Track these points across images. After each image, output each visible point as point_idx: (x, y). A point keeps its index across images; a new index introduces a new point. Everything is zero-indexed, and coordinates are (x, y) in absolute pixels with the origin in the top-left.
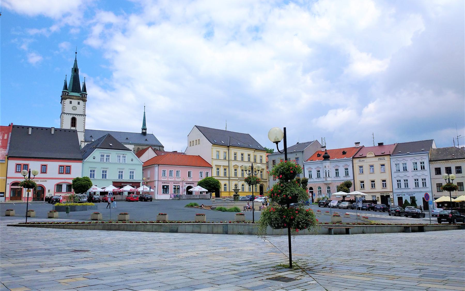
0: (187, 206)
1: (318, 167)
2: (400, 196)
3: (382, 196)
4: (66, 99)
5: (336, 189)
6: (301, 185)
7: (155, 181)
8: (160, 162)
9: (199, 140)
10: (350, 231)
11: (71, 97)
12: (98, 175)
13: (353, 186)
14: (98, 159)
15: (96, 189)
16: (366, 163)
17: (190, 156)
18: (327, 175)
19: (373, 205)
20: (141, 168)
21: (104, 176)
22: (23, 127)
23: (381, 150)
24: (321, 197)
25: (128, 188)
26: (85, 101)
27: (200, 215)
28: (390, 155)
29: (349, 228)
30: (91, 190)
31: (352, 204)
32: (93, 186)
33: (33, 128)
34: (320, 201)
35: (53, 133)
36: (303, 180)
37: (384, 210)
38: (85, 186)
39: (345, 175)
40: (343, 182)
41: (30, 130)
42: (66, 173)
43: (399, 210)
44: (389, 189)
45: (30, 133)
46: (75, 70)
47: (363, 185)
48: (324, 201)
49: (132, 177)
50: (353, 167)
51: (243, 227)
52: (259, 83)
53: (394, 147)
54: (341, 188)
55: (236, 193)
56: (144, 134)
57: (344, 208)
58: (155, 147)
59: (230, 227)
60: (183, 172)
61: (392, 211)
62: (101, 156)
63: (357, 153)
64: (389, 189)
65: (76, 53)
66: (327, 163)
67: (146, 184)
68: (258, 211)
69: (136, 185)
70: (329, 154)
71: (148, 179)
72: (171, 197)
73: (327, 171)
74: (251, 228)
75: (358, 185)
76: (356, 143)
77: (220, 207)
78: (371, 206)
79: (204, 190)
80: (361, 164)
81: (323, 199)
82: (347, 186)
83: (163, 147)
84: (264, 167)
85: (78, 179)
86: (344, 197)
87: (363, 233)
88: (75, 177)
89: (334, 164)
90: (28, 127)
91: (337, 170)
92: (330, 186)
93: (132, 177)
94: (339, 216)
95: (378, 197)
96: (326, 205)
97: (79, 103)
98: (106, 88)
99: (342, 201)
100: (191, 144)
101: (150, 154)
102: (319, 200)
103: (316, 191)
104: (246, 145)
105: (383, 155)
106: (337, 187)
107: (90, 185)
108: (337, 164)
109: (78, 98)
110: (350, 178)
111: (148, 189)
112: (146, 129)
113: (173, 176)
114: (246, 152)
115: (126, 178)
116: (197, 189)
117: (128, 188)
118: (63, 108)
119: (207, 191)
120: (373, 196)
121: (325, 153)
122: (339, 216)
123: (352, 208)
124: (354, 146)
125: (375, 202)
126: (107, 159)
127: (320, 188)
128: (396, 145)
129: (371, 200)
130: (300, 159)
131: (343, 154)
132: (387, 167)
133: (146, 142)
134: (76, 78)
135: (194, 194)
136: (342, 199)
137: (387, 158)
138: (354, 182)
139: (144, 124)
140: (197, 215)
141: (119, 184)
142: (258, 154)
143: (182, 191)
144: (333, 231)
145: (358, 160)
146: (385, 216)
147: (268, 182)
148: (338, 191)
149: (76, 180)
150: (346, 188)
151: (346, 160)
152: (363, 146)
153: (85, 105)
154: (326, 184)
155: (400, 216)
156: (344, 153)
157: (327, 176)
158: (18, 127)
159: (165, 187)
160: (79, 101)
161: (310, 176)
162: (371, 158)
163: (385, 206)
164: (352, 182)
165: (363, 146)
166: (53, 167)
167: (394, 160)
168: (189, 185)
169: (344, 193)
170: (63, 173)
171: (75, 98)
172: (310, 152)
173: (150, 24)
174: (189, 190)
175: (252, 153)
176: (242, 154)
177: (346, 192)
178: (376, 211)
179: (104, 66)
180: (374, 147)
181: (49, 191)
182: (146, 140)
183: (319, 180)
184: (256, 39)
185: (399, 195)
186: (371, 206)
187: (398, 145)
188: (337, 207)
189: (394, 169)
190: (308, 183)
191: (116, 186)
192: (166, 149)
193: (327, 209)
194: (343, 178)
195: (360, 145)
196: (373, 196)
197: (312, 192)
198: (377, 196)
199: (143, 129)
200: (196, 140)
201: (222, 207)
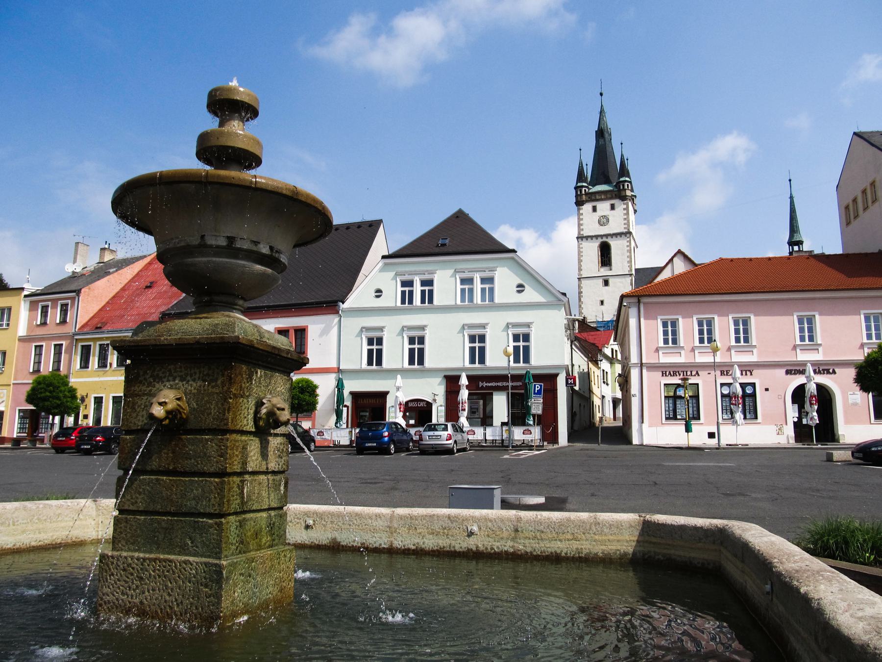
21: (417, 356)
46: (602, 134)
93: (522, 353)
112: (799, 243)
113: (682, 341)
139: (794, 228)
160: (613, 202)
164: (600, 240)
199: (791, 243)
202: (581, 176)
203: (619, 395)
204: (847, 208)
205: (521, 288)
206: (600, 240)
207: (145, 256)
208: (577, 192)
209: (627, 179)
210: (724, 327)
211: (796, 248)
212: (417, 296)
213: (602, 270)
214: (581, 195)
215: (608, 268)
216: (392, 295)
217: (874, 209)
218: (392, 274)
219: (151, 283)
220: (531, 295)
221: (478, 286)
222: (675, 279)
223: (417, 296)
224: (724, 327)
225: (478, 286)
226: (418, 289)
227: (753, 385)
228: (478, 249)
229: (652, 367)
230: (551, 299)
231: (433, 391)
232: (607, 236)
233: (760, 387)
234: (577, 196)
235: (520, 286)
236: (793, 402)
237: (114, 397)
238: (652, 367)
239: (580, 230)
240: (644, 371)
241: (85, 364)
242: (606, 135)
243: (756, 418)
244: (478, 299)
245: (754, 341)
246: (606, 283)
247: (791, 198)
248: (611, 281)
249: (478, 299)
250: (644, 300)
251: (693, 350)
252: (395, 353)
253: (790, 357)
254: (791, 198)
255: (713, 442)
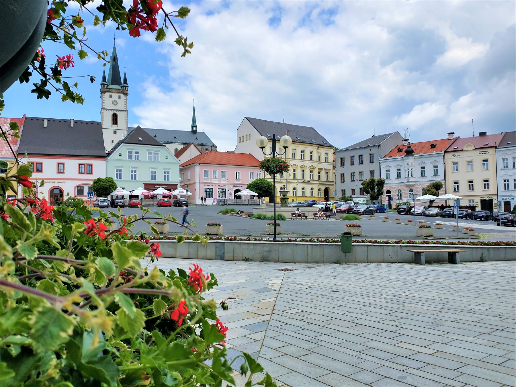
0: (221, 212)
1: (398, 165)
2: (508, 200)
3: (482, 201)
4: (105, 92)
5: (421, 192)
6: (376, 187)
7: (196, 183)
8: (202, 161)
9: (250, 135)
10: (458, 257)
11: (110, 90)
12: (126, 175)
13: (443, 188)
14: (125, 156)
15: (121, 191)
16: (462, 159)
17: (238, 154)
18: (410, 174)
19: (470, 211)
20: (178, 168)
21: (133, 177)
22: (38, 119)
23: (483, 143)
24: (401, 202)
25: (160, 191)
26: (126, 94)
27: (213, 225)
28: (496, 147)
29: (455, 252)
30: (115, 193)
31: (445, 211)
32: (119, 189)
33: (49, 120)
34: (400, 207)
35: (72, 125)
36: (378, 182)
37: (487, 218)
38: (107, 188)
39: (433, 174)
40: (431, 182)
41: (45, 122)
42: (87, 173)
43: (513, 218)
44: (492, 190)
45: (45, 126)
47: (458, 186)
48: (405, 207)
49: (167, 178)
50: (444, 164)
51: (252, 247)
52: (331, 75)
53: (502, 136)
54: (429, 190)
55: (284, 196)
56: (194, 132)
57: (432, 216)
58: (207, 147)
59: (229, 247)
60: (230, 172)
61: (502, 219)
62: (129, 152)
63: (450, 146)
64: (492, 190)
65: (114, 39)
66: (410, 160)
67: (186, 187)
68: (312, 220)
69: (171, 187)
70: (413, 148)
71: (189, 180)
72: (213, 202)
73: (410, 169)
74: (266, 249)
75: (450, 186)
76: (449, 134)
77: (259, 213)
78: (469, 213)
79: (254, 193)
80: (455, 160)
81: (404, 204)
82: (436, 188)
83: (216, 147)
84: (331, 167)
85: (99, 180)
86: (431, 202)
87: (482, 260)
88: (96, 178)
89: (419, 161)
90: (43, 119)
91: (423, 168)
92: (414, 188)
93: (167, 178)
94: (429, 227)
95: (477, 202)
96: (408, 211)
97: (119, 97)
98: (167, 89)
99: (430, 207)
100: (241, 140)
101: (192, 152)
102: (398, 206)
103: (394, 194)
104: (307, 140)
105: (487, 147)
106: (423, 189)
107: (113, 187)
108: (424, 160)
109: (119, 91)
110: (440, 178)
111: (185, 191)
112: (196, 127)
114: (307, 149)
115: (160, 179)
116: (246, 193)
117: (160, 191)
118: (103, 103)
119: (257, 194)
120: (470, 201)
121: (408, 147)
122: (429, 227)
123: (443, 216)
124: (447, 137)
125: (473, 208)
126: (135, 156)
127: (400, 191)
128: (503, 134)
129: (468, 205)
130: (375, 156)
131: (432, 148)
132: (491, 163)
133: (197, 140)
134: (115, 70)
135: (243, 198)
136: (428, 204)
137: (490, 151)
138: (445, 183)
139: (194, 121)
140: (208, 225)
141: (150, 187)
142: (323, 151)
143: (230, 197)
144: (423, 258)
145: (452, 154)
146: (492, 226)
147: (334, 185)
148: (424, 194)
149: (97, 181)
150: (434, 190)
151: (435, 155)
152: (459, 137)
153: (127, 99)
154: (408, 186)
155: (513, 226)
156: (433, 146)
157: (410, 176)
158: (32, 119)
159: (208, 190)
161: (388, 178)
162: (469, 152)
163: (489, 213)
164: (443, 182)
165: (459, 137)
166: (72, 165)
167: (500, 153)
168: (237, 188)
169: (432, 197)
170: (84, 173)
171: (115, 91)
172: (389, 146)
173: (210, 13)
174: (236, 194)
175: (314, 149)
176: (303, 152)
177: (434, 195)
178: (476, 219)
179: (160, 63)
180: (474, 138)
181: (68, 194)
182: (196, 139)
183: (400, 181)
184: (328, 23)
185: (506, 199)
186: (469, 213)
187: (507, 134)
188: (423, 214)
189: (501, 165)
190: (385, 185)
191: (145, 189)
192: (218, 150)
193: (409, 217)
194: (430, 179)
195: (455, 136)
196: (470, 201)
197: (390, 196)
198: (475, 201)
199: (193, 126)
200: (247, 135)
201: (262, 213)
210: (219, 173)
213: (114, 125)
221: (153, 155)
224: (219, 173)
225: (153, 155)
226: (134, 154)
232: (117, 110)
239: (102, 105)
244: (153, 160)
246: (115, 133)
248: (117, 131)
249: (153, 160)
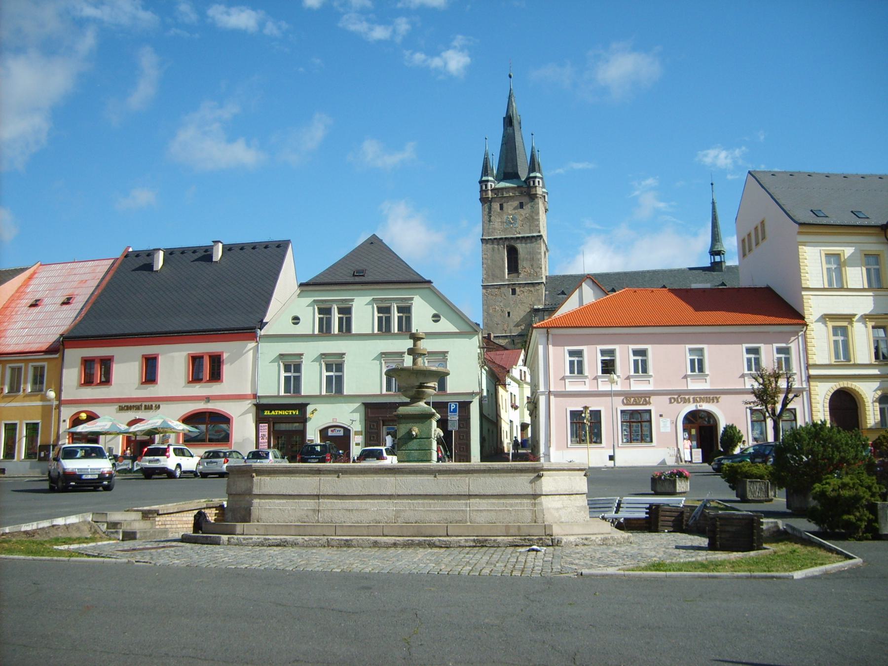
113: (586, 372)
164: (507, 243)
199: (714, 253)
202: (486, 170)
203: (528, 420)
204: (743, 241)
205: (436, 318)
206: (507, 243)
207: (23, 270)
208: (481, 187)
209: (538, 175)
211: (718, 258)
212: (334, 323)
214: (486, 191)
215: (515, 275)
216: (310, 322)
217: (763, 245)
218: (310, 300)
219: (37, 301)
220: (446, 325)
222: (584, 311)
223: (334, 323)
227: (649, 411)
228: (395, 279)
229: (558, 395)
230: (468, 329)
231: (349, 416)
233: (656, 412)
234: (481, 191)
235: (435, 316)
236: (684, 430)
237: (600, 411)
238: (558, 395)
240: (552, 397)
241: (15, 388)
242: (515, 123)
243: (651, 441)
245: (651, 371)
247: (713, 203)
250: (551, 331)
251: (596, 378)
252: (313, 381)
253: (680, 386)
254: (713, 203)
255: (611, 464)
